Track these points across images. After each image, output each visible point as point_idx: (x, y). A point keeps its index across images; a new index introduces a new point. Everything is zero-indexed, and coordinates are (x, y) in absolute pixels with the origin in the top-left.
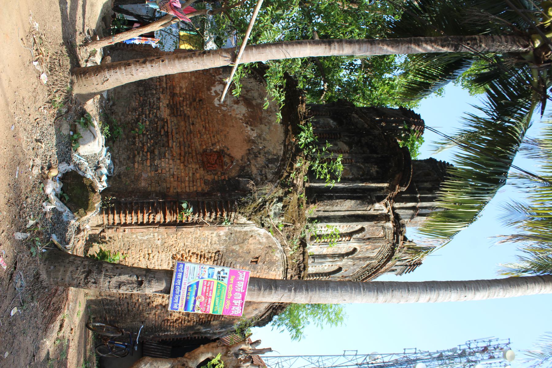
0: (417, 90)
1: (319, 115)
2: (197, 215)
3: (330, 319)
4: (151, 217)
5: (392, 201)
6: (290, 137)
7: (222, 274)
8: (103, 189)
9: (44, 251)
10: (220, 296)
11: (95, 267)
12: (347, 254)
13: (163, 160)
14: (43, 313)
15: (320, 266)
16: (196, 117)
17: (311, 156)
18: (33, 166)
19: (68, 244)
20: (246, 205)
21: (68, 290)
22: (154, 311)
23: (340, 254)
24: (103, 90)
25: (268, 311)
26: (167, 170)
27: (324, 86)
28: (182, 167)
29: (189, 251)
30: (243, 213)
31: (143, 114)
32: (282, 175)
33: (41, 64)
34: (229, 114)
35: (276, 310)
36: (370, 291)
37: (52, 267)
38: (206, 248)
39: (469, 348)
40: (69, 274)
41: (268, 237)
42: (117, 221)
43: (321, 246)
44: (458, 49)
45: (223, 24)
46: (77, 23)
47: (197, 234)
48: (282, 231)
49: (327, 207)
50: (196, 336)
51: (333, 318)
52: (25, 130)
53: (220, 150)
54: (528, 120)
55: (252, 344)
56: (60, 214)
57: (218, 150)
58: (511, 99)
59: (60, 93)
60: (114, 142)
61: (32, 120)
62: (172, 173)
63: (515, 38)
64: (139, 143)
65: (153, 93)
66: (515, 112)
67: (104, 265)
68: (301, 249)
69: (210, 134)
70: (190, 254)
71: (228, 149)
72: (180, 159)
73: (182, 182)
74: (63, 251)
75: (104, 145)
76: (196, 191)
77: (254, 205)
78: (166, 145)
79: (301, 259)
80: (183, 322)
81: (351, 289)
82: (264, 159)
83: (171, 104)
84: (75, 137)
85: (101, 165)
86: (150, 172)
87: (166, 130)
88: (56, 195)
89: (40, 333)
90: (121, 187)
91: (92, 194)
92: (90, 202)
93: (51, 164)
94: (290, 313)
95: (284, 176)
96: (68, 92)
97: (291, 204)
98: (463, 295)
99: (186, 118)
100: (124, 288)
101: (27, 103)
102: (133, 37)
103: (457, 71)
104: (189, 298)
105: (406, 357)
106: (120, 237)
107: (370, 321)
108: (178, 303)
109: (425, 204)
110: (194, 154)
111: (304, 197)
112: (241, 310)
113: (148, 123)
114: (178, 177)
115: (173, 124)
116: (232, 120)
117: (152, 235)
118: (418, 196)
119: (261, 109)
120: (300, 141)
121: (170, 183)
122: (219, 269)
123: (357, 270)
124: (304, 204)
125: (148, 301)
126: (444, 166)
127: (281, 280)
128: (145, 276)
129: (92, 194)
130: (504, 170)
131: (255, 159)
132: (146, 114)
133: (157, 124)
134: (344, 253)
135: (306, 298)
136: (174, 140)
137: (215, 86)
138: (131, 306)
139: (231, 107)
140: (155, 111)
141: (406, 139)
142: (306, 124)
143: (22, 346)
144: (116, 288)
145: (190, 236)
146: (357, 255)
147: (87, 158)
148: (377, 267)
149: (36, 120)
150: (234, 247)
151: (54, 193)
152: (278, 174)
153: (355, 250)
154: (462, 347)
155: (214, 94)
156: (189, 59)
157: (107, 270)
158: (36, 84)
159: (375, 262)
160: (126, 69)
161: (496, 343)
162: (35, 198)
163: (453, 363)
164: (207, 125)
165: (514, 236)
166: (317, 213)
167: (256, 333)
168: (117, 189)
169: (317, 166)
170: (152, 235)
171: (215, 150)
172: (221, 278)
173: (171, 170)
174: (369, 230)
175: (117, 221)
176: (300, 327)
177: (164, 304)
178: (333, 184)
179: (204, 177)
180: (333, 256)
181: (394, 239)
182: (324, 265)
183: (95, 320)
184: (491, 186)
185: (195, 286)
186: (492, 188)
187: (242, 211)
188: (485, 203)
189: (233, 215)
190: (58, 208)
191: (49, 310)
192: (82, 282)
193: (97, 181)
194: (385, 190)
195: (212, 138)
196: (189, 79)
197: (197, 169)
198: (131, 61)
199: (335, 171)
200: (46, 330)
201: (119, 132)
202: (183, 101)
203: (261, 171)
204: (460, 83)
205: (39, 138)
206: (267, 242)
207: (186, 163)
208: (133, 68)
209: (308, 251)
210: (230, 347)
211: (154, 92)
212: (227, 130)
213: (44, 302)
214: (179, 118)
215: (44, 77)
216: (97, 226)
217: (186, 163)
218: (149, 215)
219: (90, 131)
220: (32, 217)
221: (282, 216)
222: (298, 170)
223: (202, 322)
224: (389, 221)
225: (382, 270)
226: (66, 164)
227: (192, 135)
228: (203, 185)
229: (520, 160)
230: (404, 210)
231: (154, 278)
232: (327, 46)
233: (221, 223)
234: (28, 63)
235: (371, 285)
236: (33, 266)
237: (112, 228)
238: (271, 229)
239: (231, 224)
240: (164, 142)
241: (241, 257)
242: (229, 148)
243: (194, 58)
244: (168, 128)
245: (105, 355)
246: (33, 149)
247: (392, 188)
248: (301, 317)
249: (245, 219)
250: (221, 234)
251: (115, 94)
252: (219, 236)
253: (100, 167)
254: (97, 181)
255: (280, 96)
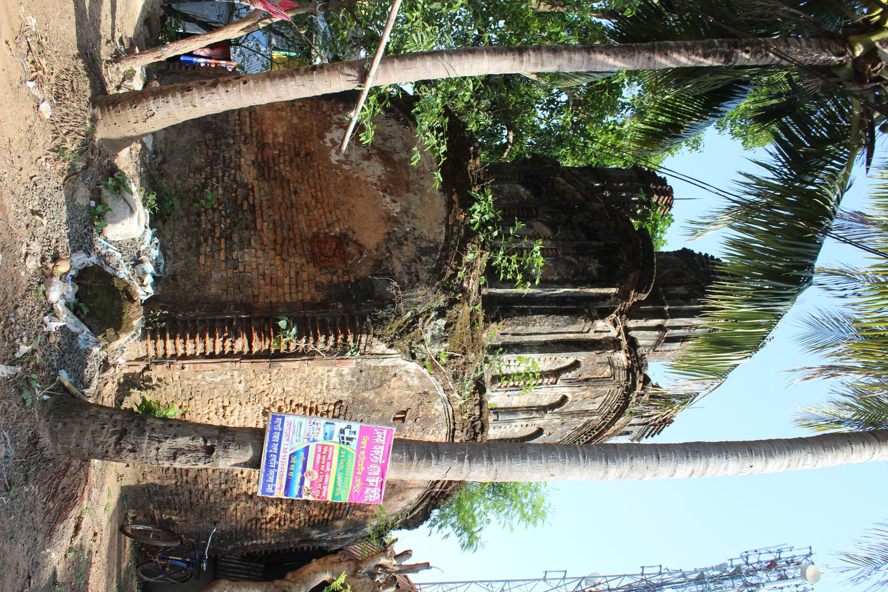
0: (667, 132)
1: (501, 179)
2: (304, 340)
3: (524, 515)
4: (228, 343)
5: (624, 316)
6: (455, 212)
7: (347, 434)
8: (146, 298)
9: (45, 397)
10: (344, 471)
11: (133, 425)
12: (552, 406)
13: (246, 250)
14: (45, 504)
15: (508, 427)
16: (300, 181)
17: (490, 243)
18: (27, 255)
19: (87, 387)
20: (385, 322)
21: (89, 466)
22: (234, 504)
23: (539, 406)
24: (145, 132)
25: (423, 501)
26: (254, 266)
27: (507, 136)
28: (278, 262)
29: (291, 401)
30: (380, 336)
31: (213, 176)
32: (445, 273)
33: (40, 86)
34: (355, 176)
35: (436, 499)
36: (594, 459)
37: (60, 425)
38: (319, 396)
39: (747, 563)
40: (88, 436)
41: (422, 377)
42: (170, 352)
43: (508, 393)
44: (730, 61)
45: (344, 29)
46: (103, 24)
47: (304, 372)
48: (445, 366)
49: (519, 328)
50: (305, 545)
51: (530, 512)
52: (13, 193)
53: (341, 234)
54: (846, 177)
55: (396, 557)
56: (75, 336)
57: (338, 235)
58: (813, 149)
59: (73, 135)
60: (164, 222)
61: (26, 178)
62: (261, 271)
63: (823, 41)
64: (206, 224)
65: (229, 143)
66: (822, 168)
67: (149, 421)
68: (477, 396)
69: (323, 209)
70: (293, 406)
71: (354, 232)
72: (275, 249)
73: (278, 286)
74: (79, 398)
75: (148, 225)
76: (302, 300)
77: (400, 322)
78: (252, 226)
79: (477, 413)
80: (282, 523)
81: (564, 457)
82: (414, 249)
83: (260, 160)
84: (100, 209)
85: (143, 257)
86: (226, 270)
87: (251, 202)
88: (67, 305)
89: (39, 539)
90: (177, 294)
91: (128, 305)
92: (125, 317)
93: (58, 253)
94: (460, 506)
95: (448, 275)
96: (87, 135)
97: (460, 321)
98: (747, 465)
99: (283, 182)
100: (183, 458)
101: (16, 148)
102: (197, 45)
103: (725, 104)
104: (292, 474)
105: (645, 580)
106: (176, 378)
107: (591, 513)
108: (274, 482)
109: (677, 322)
110: (298, 241)
111: (480, 310)
112: (381, 493)
113: (221, 191)
114: (271, 278)
115: (262, 192)
116: (360, 185)
117: (229, 374)
118: (666, 308)
119: (407, 168)
120: (472, 218)
121: (259, 288)
122: (340, 424)
123: (568, 434)
124: (481, 322)
125: (223, 486)
126: (706, 261)
127: (446, 443)
128: (218, 438)
129: (128, 305)
130: (810, 262)
131: (399, 249)
132: (217, 177)
133: (236, 192)
134: (547, 404)
135: (488, 472)
136: (265, 218)
137: (331, 132)
138: (196, 496)
139: (358, 165)
140: (233, 172)
141: (644, 217)
142: (481, 191)
143: (8, 560)
144: (169, 458)
145: (293, 375)
146: (567, 407)
147: (119, 246)
148: (600, 427)
149: (31, 178)
150: (366, 395)
151: (63, 302)
152: (437, 272)
153: (564, 399)
154: (735, 563)
155: (329, 144)
156: (288, 79)
157: (153, 429)
158: (33, 118)
159: (597, 420)
160: (183, 96)
161: (790, 554)
162: (30, 309)
163: (721, 588)
164: (319, 194)
165: (825, 369)
166: (502, 337)
167: (402, 539)
168: (170, 298)
169: (500, 259)
170: (229, 374)
171: (332, 234)
172: (346, 441)
173: (261, 267)
174: (587, 365)
175: (170, 352)
176: (475, 529)
177: (250, 493)
178: (527, 290)
179: (315, 278)
180: (529, 409)
181: (628, 380)
182: (513, 424)
183: (135, 521)
184: (788, 288)
185: (303, 454)
186: (789, 291)
187: (379, 332)
188: (778, 317)
189: (364, 339)
190: (69, 326)
191: (56, 500)
192: (111, 450)
193: (136, 283)
194: (613, 299)
195: (328, 215)
196: (289, 121)
197: (303, 265)
198: (191, 84)
199: (530, 268)
200: (50, 533)
201: (172, 205)
202: (279, 155)
203: (409, 268)
204: (728, 130)
205: (37, 208)
206: (420, 385)
207: (285, 256)
208: (195, 95)
209: (489, 402)
210: (362, 562)
211: (232, 141)
212: (353, 201)
213: (46, 486)
214: (272, 182)
215: (45, 107)
216: (137, 360)
217: (285, 256)
218: (224, 341)
219: (125, 200)
220: (25, 339)
221: (446, 341)
222: (470, 266)
223: (314, 521)
224: (620, 349)
225: (609, 432)
226: (84, 255)
227: (294, 210)
228: (313, 290)
229: (832, 253)
230: (644, 332)
231: (233, 441)
232: (517, 56)
233: (344, 352)
234: (17, 83)
235: (596, 449)
236: (27, 423)
237: (163, 363)
238: (427, 363)
239: (361, 354)
240: (248, 222)
241: (378, 411)
242: (356, 230)
243: (297, 77)
244: (254, 199)
245: (152, 580)
246: (27, 226)
247: (624, 296)
248: (476, 512)
249: (384, 345)
250: (343, 373)
251: (166, 144)
252: (342, 375)
253: (141, 262)
254: (136, 284)
255: (439, 145)
